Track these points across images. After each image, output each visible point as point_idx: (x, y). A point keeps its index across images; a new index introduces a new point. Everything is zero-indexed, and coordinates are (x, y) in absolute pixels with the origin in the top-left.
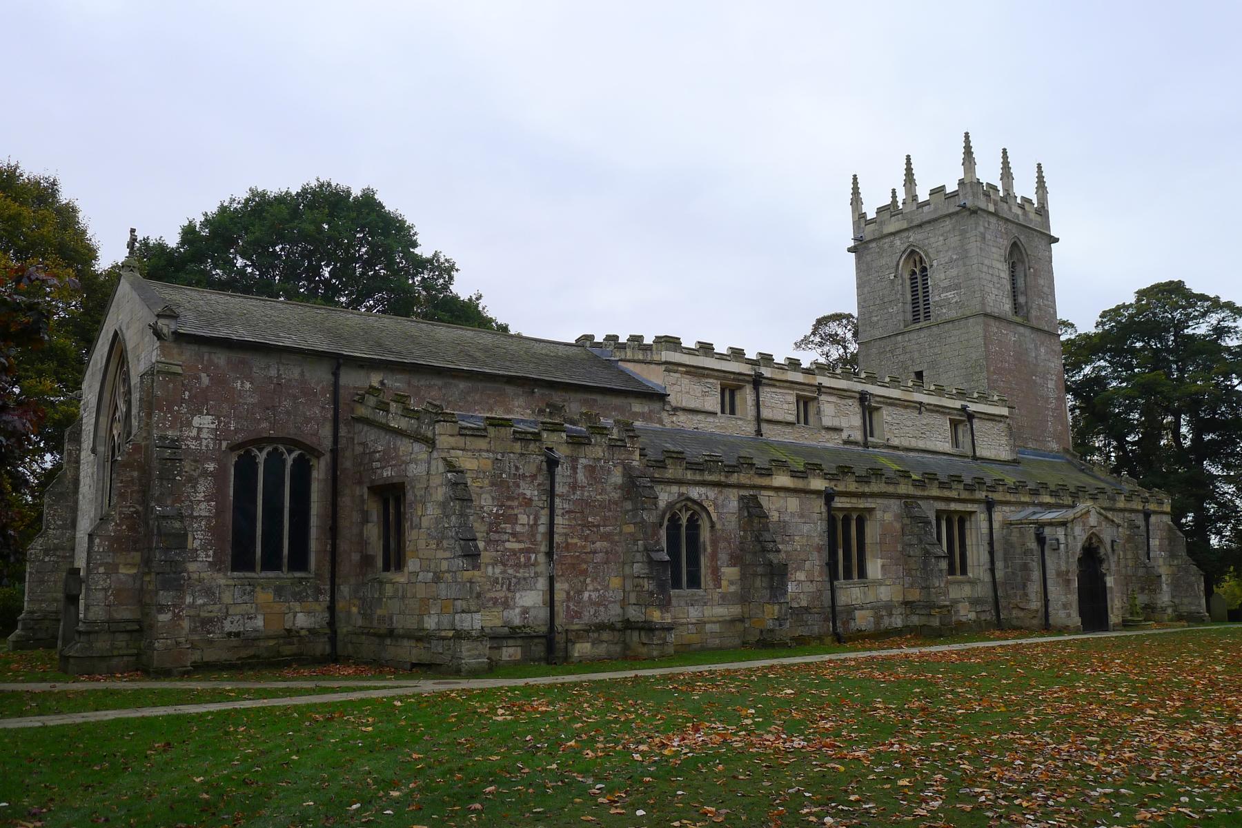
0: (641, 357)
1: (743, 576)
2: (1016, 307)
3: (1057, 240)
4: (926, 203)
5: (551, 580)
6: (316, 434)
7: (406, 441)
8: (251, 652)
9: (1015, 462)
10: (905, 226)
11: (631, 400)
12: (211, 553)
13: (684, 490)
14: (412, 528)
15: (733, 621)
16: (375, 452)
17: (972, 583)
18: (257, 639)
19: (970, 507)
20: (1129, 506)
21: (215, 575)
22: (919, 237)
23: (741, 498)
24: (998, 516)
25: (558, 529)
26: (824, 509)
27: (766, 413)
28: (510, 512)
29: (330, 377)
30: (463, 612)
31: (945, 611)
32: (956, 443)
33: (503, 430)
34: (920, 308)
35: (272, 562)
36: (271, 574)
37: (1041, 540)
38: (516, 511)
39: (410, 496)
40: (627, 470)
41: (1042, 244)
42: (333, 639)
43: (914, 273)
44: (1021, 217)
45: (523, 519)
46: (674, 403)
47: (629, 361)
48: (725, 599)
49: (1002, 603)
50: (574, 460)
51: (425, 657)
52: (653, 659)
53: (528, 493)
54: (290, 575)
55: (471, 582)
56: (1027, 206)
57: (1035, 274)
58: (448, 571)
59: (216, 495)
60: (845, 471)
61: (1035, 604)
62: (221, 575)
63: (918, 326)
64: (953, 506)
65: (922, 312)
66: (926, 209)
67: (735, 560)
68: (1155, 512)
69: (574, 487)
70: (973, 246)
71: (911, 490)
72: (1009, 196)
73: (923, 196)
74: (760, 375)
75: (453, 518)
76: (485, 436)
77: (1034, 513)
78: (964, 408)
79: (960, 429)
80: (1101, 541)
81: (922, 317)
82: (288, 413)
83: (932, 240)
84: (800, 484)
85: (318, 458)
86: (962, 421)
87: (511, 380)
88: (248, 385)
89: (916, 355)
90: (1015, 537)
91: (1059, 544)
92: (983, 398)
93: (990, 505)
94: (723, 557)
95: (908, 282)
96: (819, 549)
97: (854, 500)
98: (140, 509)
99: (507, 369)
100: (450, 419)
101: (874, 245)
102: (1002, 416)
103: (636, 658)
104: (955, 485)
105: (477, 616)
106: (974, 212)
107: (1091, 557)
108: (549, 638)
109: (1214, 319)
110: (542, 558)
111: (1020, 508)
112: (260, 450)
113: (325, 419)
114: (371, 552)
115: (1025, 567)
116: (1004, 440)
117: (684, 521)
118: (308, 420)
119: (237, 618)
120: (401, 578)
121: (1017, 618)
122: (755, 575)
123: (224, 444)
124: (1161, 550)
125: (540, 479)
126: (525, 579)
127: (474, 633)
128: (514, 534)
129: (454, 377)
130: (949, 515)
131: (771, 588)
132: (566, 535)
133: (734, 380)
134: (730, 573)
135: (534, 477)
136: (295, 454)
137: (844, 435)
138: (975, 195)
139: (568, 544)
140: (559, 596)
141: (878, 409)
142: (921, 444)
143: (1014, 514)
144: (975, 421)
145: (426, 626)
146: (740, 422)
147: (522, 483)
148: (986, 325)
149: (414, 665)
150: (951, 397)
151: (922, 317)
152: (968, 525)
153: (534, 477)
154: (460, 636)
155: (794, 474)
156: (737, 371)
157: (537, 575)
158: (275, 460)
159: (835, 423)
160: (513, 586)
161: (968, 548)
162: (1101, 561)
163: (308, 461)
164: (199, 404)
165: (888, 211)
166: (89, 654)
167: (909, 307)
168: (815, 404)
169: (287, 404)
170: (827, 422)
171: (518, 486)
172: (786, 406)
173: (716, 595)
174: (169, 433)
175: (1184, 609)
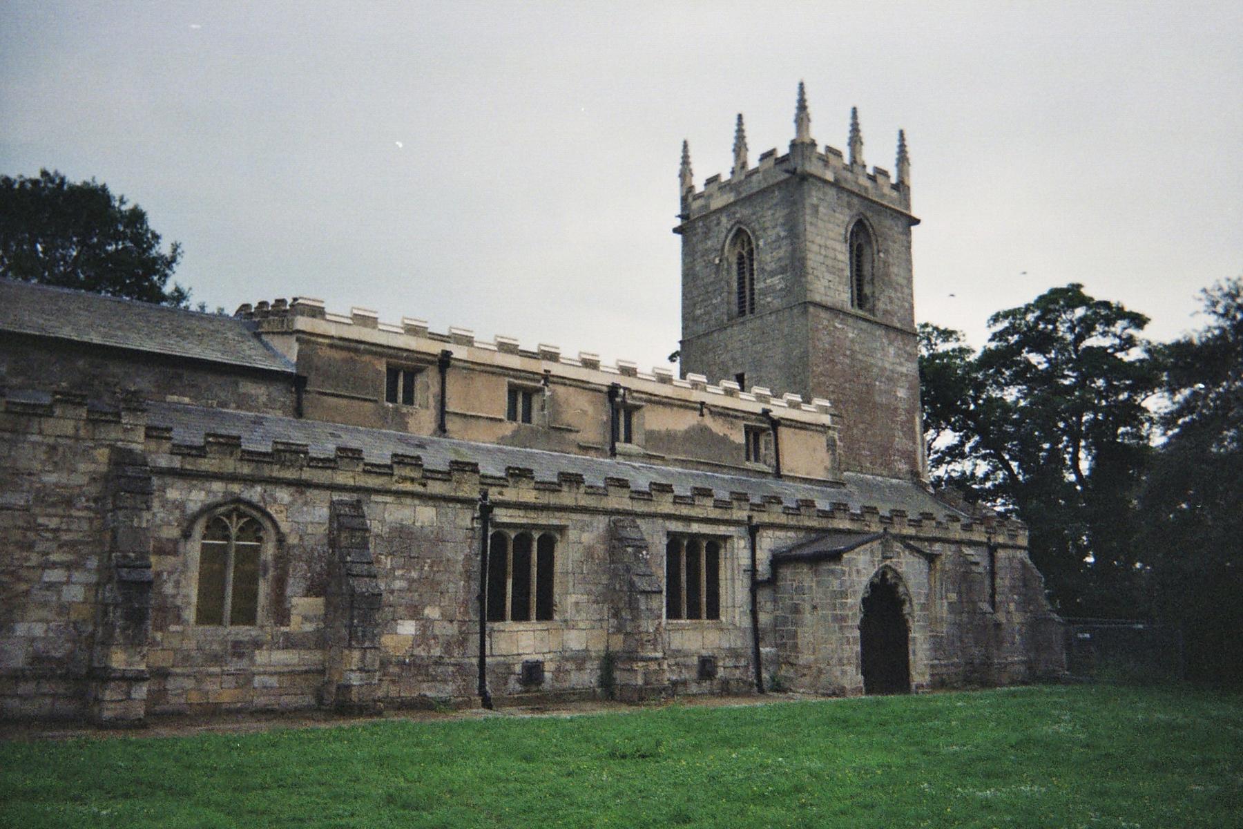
2: (860, 299)
3: (917, 222)
4: (756, 171)
19: (722, 530)
20: (965, 536)
27: (451, 408)
31: (653, 666)
56: (880, 179)
64: (695, 528)
66: (754, 178)
68: (1004, 546)
71: (627, 504)
74: (447, 354)
78: (766, 413)
79: (762, 440)
80: (898, 576)
86: (764, 430)
93: (753, 531)
95: (735, 267)
97: (532, 514)
102: (823, 426)
130: (695, 538)
133: (406, 358)
141: (638, 408)
167: (734, 298)
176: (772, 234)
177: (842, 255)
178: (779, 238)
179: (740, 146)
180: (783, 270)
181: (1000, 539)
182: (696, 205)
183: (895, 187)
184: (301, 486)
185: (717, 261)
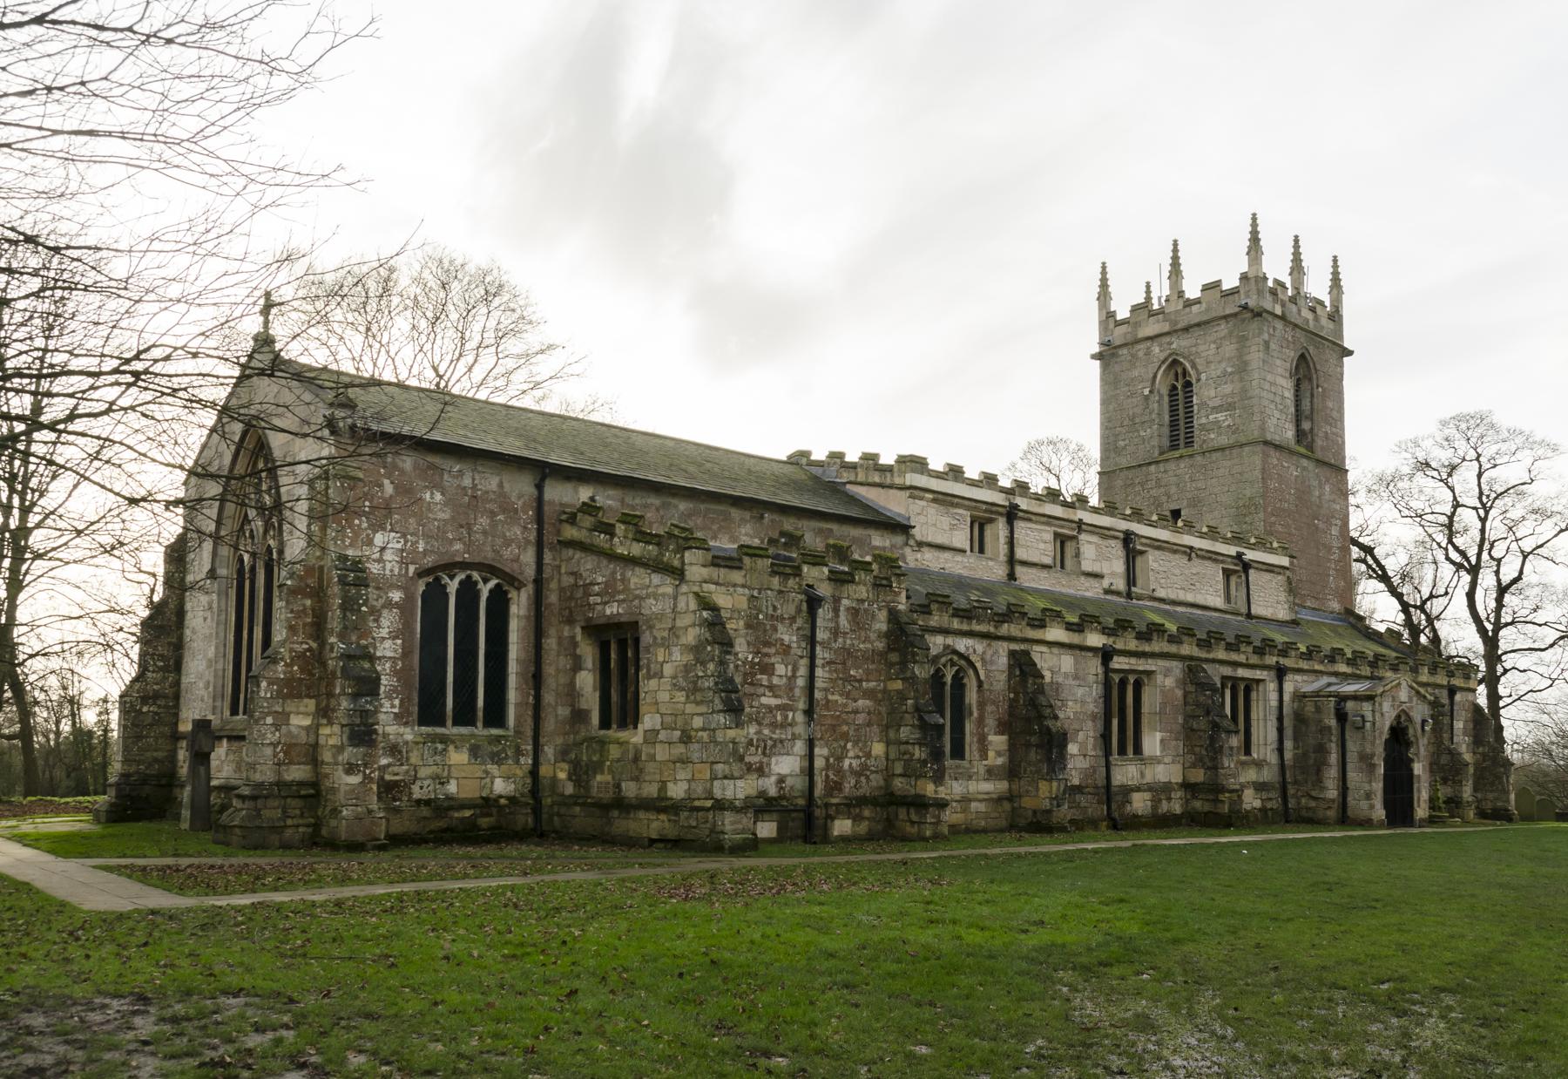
0: (877, 479)
1: (1012, 747)
2: (1300, 435)
3: (1350, 353)
4: (1197, 301)
5: (811, 744)
6: (517, 560)
7: (639, 570)
8: (442, 824)
9: (1295, 622)
10: (1166, 327)
11: (872, 532)
12: (397, 702)
13: (950, 641)
14: (649, 677)
15: (1000, 800)
16: (592, 584)
17: (1259, 764)
18: (451, 808)
19: (1258, 674)
20: (1432, 680)
21: (402, 730)
22: (1184, 343)
23: (1012, 654)
24: (1289, 687)
25: (819, 684)
26: (1100, 670)
27: (1020, 554)
28: (766, 660)
29: (533, 491)
30: (725, 777)
32: (1228, 598)
33: (759, 561)
35: (464, 715)
36: (464, 730)
37: (1342, 717)
38: (773, 660)
39: (646, 638)
40: (893, 615)
41: (1331, 356)
42: (537, 810)
43: (1174, 388)
44: (1311, 323)
45: (780, 669)
46: (918, 538)
47: (861, 484)
48: (991, 773)
49: (1291, 791)
50: (837, 601)
51: (671, 832)
52: (925, 839)
53: (786, 638)
54: (486, 732)
55: (734, 743)
56: (1319, 309)
57: (1324, 396)
58: (704, 729)
59: (402, 632)
60: (1122, 625)
61: (1332, 793)
62: (408, 730)
63: (1177, 454)
64: (1241, 672)
65: (1182, 437)
66: (1195, 308)
67: (1004, 727)
68: (1462, 689)
69: (836, 632)
70: (1255, 356)
75: (711, 666)
76: (740, 568)
77: (1329, 685)
78: (1239, 556)
79: (1233, 579)
80: (1409, 719)
81: (1182, 442)
82: (485, 533)
83: (1201, 348)
84: (1075, 638)
85: (518, 589)
87: (737, 502)
88: (438, 497)
89: (1173, 490)
90: (1310, 708)
91: (1364, 721)
92: (1261, 545)
93: (1281, 672)
94: (991, 722)
95: (1166, 399)
96: (1094, 717)
97: (1133, 660)
98: (314, 645)
99: (733, 488)
100: (702, 545)
101: (1125, 351)
103: (905, 839)
104: (1243, 647)
105: (740, 783)
106: (1258, 314)
107: (1399, 736)
108: (808, 813)
109: (1526, 457)
110: (800, 717)
111: (1312, 678)
112: (452, 577)
113: (528, 542)
114: (584, 706)
115: (1322, 750)
116: (1283, 596)
117: (949, 679)
118: (508, 543)
119: (426, 783)
120: (636, 737)
121: (1308, 809)
122: (1028, 745)
123: (412, 569)
124: (1465, 734)
125: (799, 622)
126: (781, 741)
127: (737, 803)
128: (771, 687)
129: (674, 495)
130: (1235, 681)
131: (1049, 760)
132: (826, 690)
134: (998, 741)
135: (793, 619)
136: (493, 583)
137: (1106, 583)
138: (1260, 292)
139: (828, 701)
140: (819, 763)
141: (1142, 553)
142: (1190, 598)
143: (1310, 685)
144: (1251, 572)
145: (670, 794)
146: (991, 563)
147: (780, 627)
148: (1266, 455)
149: (652, 842)
150: (1226, 541)
151: (1182, 442)
152: (1254, 695)
153: (793, 619)
154: (720, 806)
155: (1069, 627)
156: (989, 500)
157: (795, 737)
159: (1096, 568)
160: (771, 748)
161: (1254, 723)
162: (1408, 744)
163: (506, 593)
164: (382, 515)
165: (1142, 309)
166: (257, 823)
167: (1166, 431)
168: (1074, 543)
169: (484, 521)
170: (1087, 566)
171: (776, 630)
172: (1042, 546)
173: (980, 767)
174: (350, 552)
175: (1488, 806)
176: (1215, 370)
177: (1286, 387)
178: (1225, 374)
185: (1146, 392)
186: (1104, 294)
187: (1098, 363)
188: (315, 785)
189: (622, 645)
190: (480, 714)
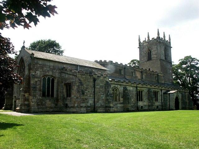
2: (165, 58)
20: (183, 91)
34: (150, 58)
35: (48, 95)
61: (168, 106)
64: (156, 90)
72: (165, 39)
73: (151, 39)
93: (161, 90)
112: (47, 77)
134: (121, 99)
158: (49, 78)
165: (145, 41)
179: (148, 37)
180: (156, 54)
181: (186, 91)
182: (141, 44)
183: (169, 43)
184: (120, 85)
186: (139, 40)
187: (139, 49)
188: (29, 104)
189: (69, 86)
190: (50, 95)
